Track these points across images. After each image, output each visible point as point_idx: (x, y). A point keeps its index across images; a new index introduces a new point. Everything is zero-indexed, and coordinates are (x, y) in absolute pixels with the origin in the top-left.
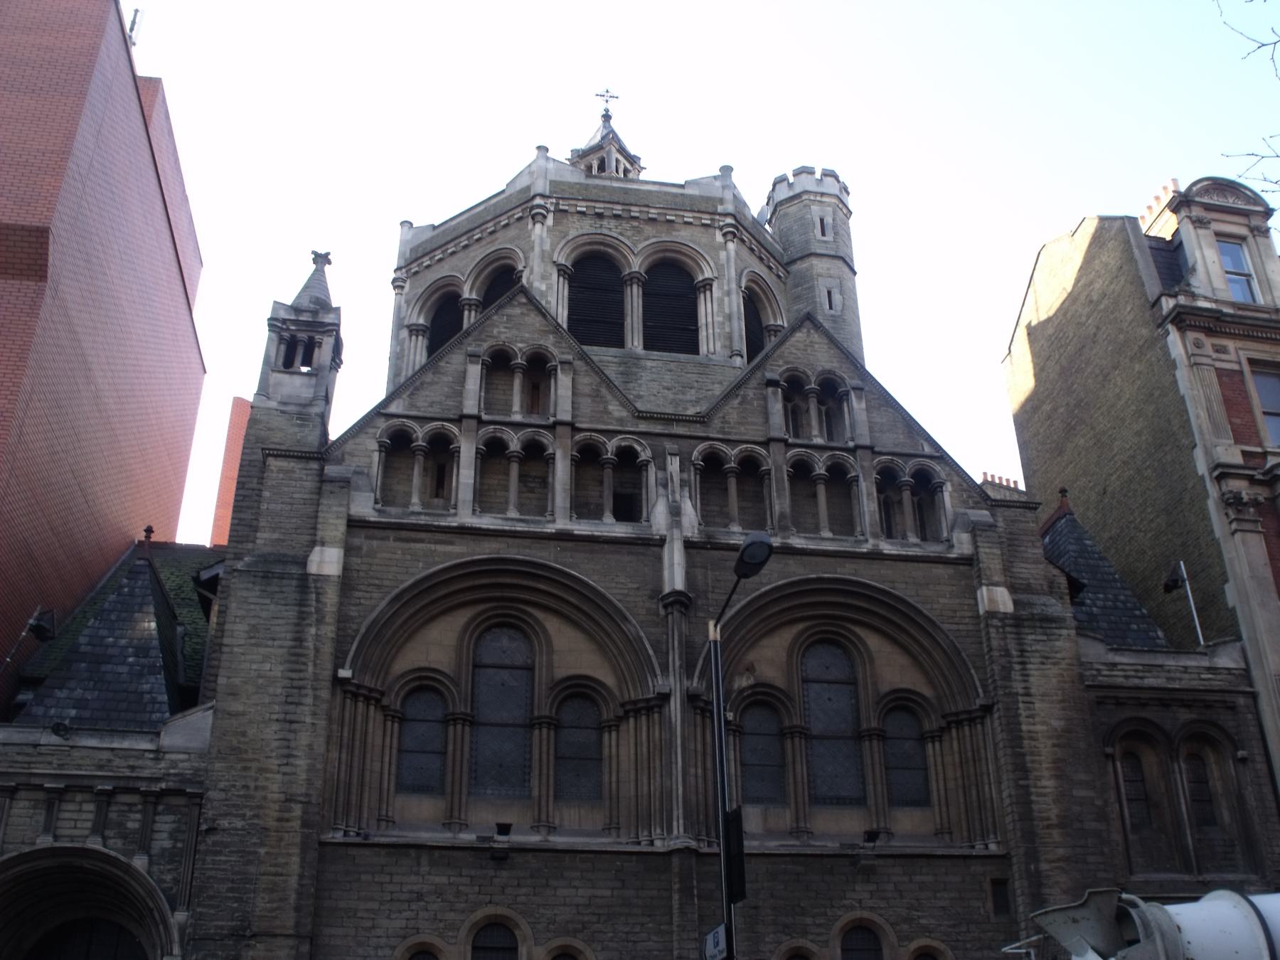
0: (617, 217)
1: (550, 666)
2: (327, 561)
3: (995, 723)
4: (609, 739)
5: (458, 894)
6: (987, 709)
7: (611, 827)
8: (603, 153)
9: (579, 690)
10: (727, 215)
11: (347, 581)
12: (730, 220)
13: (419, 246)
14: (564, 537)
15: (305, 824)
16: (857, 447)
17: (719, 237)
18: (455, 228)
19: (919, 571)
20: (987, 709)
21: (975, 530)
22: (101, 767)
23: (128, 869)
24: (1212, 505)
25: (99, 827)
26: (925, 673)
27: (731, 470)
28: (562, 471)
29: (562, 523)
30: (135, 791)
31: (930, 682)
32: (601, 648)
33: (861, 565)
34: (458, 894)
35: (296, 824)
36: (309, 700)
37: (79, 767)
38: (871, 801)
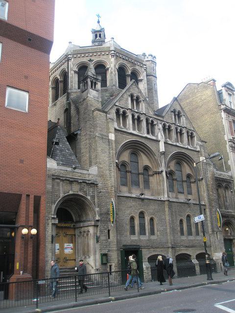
0: (123, 59)
1: (143, 163)
2: (112, 136)
3: (204, 181)
4: (151, 178)
5: (137, 206)
6: (202, 179)
7: (152, 195)
8: (101, 33)
9: (146, 168)
10: (112, 51)
11: (116, 141)
12: (113, 52)
13: (76, 50)
14: (146, 138)
15: (115, 192)
16: (143, 114)
17: (110, 57)
18: (88, 49)
19: (193, 152)
20: (202, 179)
21: (201, 146)
22: (79, 177)
23: (86, 199)
24: (228, 146)
25: (81, 190)
26: (192, 171)
27: (121, 114)
28: (185, 135)
29: (146, 135)
30: (86, 183)
31: (192, 172)
32: (150, 160)
33: (186, 150)
34: (137, 206)
35: (113, 191)
36: (113, 166)
37: (76, 176)
38: (185, 193)
